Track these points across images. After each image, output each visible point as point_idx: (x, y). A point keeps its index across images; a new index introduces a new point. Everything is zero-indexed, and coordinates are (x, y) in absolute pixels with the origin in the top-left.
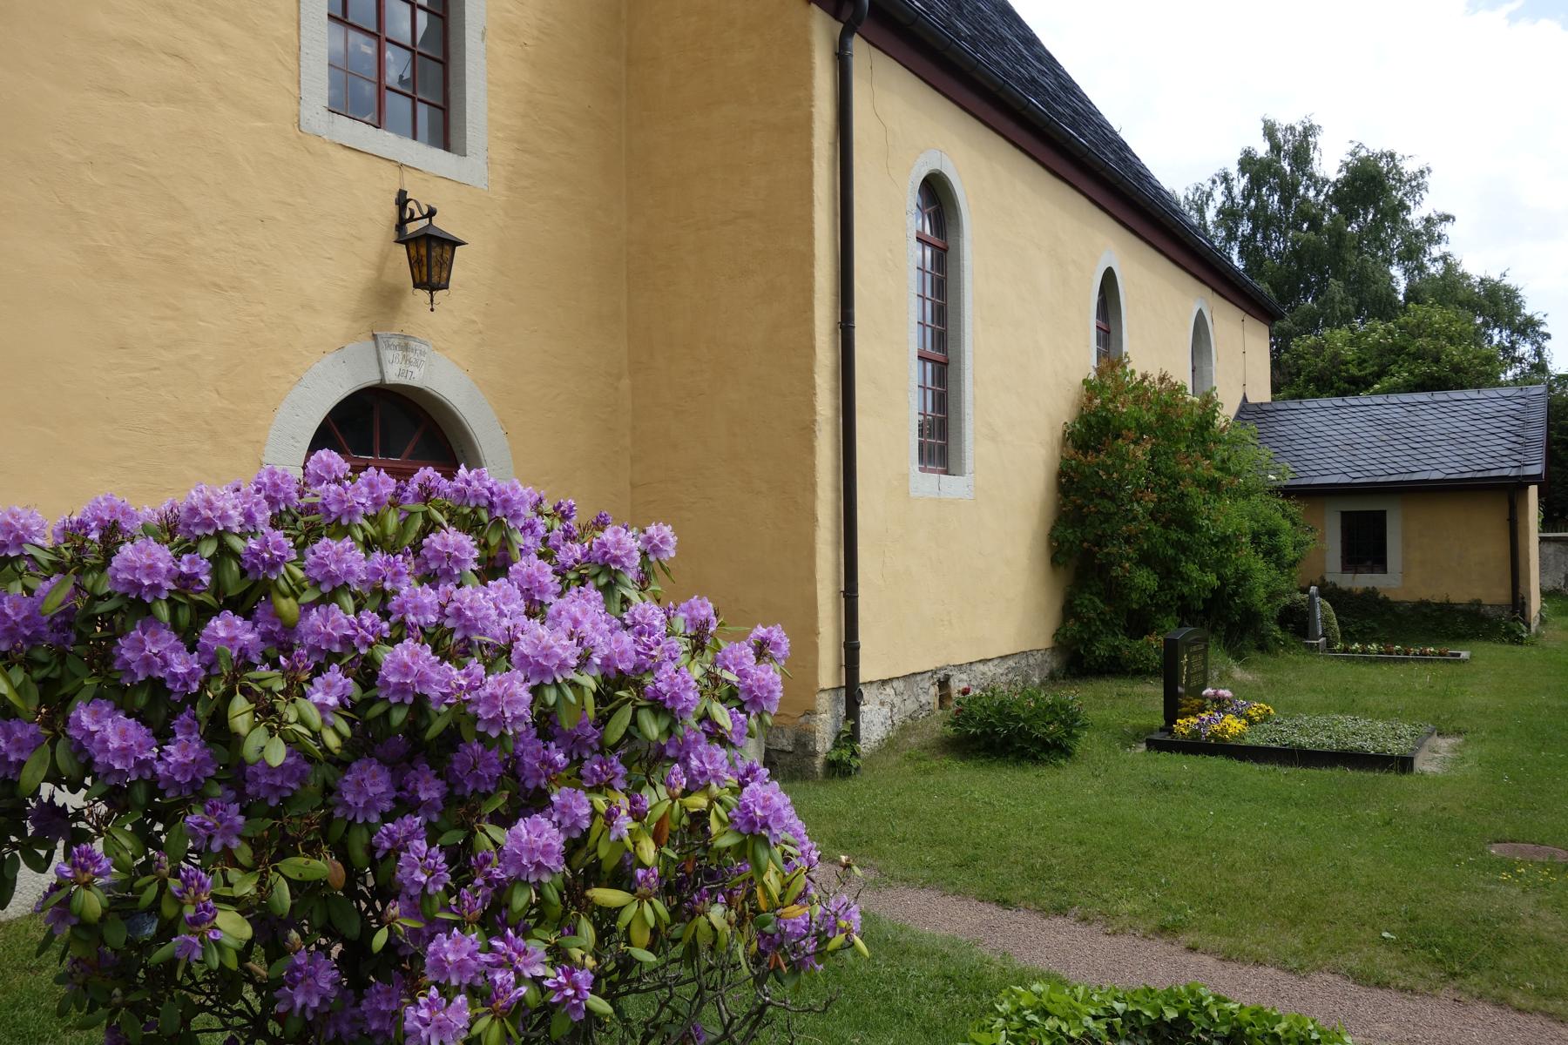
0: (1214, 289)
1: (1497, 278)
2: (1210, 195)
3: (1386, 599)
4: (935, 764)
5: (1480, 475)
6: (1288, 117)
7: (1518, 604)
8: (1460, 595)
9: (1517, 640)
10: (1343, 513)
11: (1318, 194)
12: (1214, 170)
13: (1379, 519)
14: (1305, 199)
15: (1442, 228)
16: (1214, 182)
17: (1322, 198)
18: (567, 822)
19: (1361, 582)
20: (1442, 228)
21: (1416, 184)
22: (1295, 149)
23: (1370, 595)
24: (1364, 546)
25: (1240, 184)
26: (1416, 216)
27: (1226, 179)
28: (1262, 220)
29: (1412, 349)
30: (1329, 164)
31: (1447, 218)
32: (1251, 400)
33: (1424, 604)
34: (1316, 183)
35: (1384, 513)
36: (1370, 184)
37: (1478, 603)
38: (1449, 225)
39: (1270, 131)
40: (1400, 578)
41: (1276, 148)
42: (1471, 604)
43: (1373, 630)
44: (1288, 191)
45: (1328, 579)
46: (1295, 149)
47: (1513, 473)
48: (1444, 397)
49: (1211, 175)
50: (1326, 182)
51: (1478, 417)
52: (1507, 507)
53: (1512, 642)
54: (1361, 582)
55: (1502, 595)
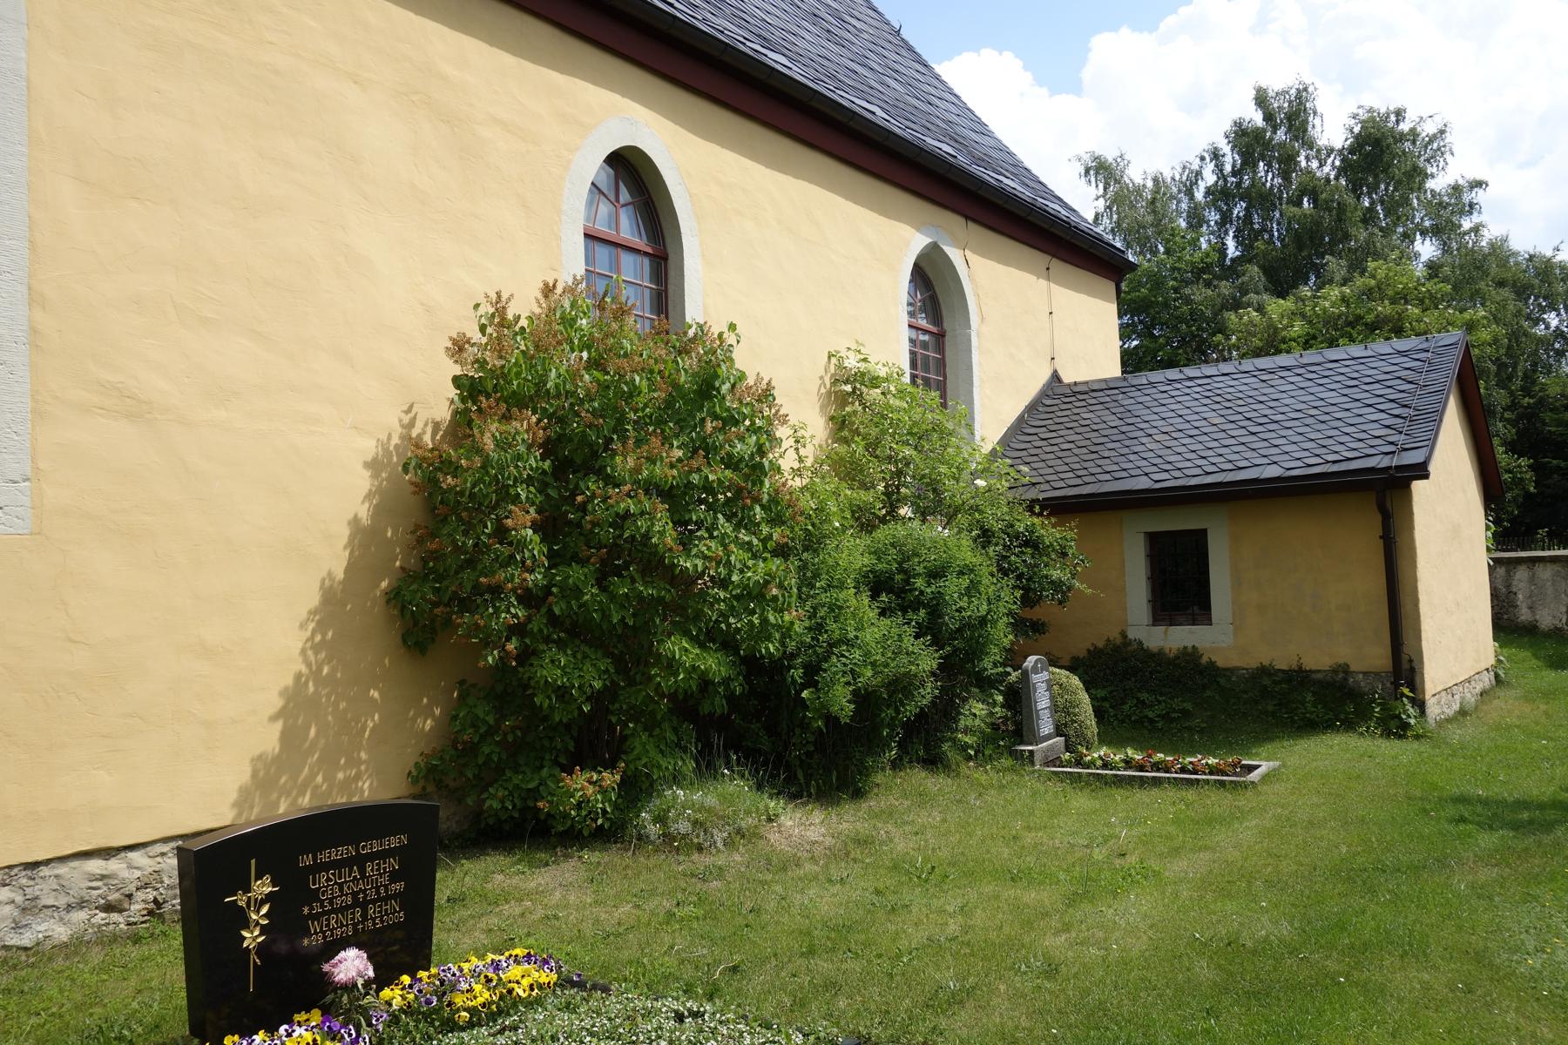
0: (967, 218)
1: (1549, 253)
2: (1198, 174)
3: (1212, 664)
4: (135, 1005)
5: (1335, 468)
6: (1279, 81)
7: (1405, 670)
8: (1318, 659)
9: (1396, 728)
10: (1153, 539)
11: (1321, 166)
12: (1201, 145)
13: (1198, 541)
14: (1309, 172)
15: (1479, 196)
16: (1203, 159)
17: (1327, 169)
18: (953, 873)
19: (1176, 638)
20: (1479, 196)
21: (1435, 146)
22: (1290, 115)
23: (1189, 659)
24: (1180, 584)
25: (1230, 159)
26: (1438, 183)
27: (1216, 155)
28: (1261, 200)
29: (1370, 318)
30: (1333, 129)
31: (1479, 184)
32: (1067, 378)
33: (1264, 671)
34: (1319, 151)
35: (1204, 532)
36: (1382, 154)
37: (1345, 669)
38: (1480, 191)
39: (1261, 100)
40: (1226, 637)
41: (1269, 117)
42: (1335, 671)
43: (1186, 714)
44: (1287, 162)
45: (1131, 635)
46: (1290, 115)
47: (1385, 462)
48: (1319, 359)
49: (1198, 152)
50: (1330, 151)
51: (1355, 382)
52: (1379, 518)
53: (1387, 734)
54: (1176, 638)
55: (1373, 656)
